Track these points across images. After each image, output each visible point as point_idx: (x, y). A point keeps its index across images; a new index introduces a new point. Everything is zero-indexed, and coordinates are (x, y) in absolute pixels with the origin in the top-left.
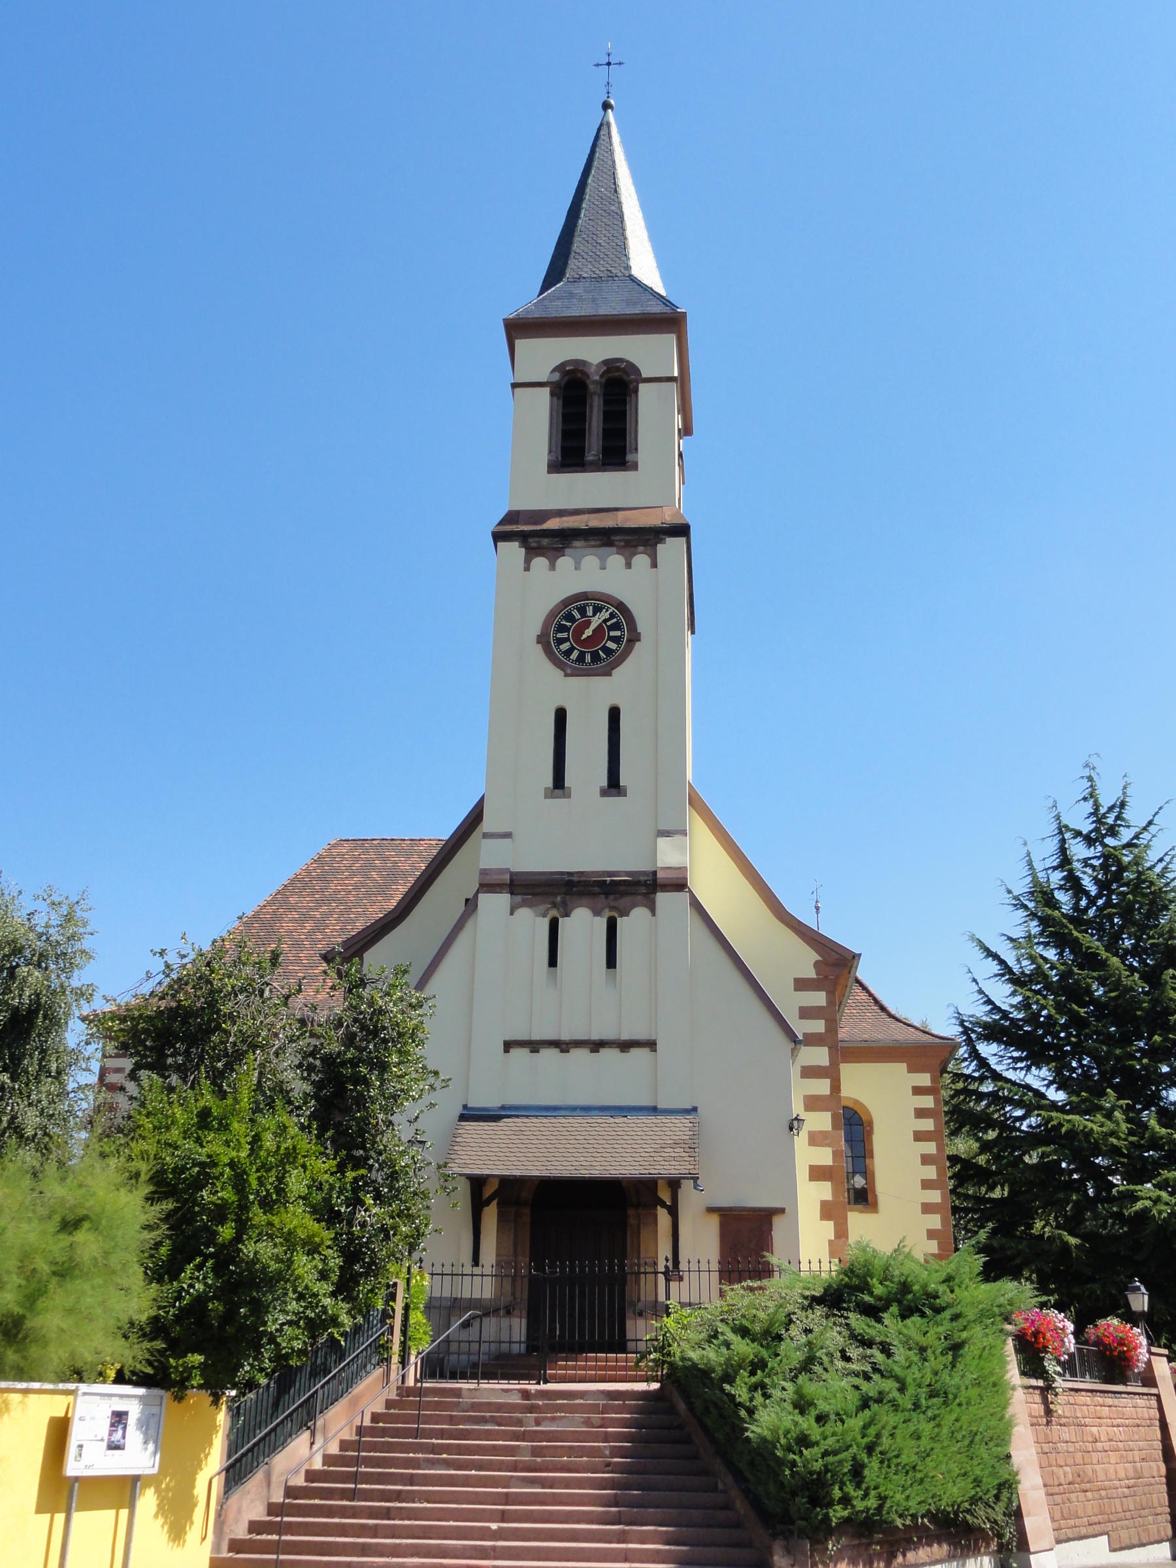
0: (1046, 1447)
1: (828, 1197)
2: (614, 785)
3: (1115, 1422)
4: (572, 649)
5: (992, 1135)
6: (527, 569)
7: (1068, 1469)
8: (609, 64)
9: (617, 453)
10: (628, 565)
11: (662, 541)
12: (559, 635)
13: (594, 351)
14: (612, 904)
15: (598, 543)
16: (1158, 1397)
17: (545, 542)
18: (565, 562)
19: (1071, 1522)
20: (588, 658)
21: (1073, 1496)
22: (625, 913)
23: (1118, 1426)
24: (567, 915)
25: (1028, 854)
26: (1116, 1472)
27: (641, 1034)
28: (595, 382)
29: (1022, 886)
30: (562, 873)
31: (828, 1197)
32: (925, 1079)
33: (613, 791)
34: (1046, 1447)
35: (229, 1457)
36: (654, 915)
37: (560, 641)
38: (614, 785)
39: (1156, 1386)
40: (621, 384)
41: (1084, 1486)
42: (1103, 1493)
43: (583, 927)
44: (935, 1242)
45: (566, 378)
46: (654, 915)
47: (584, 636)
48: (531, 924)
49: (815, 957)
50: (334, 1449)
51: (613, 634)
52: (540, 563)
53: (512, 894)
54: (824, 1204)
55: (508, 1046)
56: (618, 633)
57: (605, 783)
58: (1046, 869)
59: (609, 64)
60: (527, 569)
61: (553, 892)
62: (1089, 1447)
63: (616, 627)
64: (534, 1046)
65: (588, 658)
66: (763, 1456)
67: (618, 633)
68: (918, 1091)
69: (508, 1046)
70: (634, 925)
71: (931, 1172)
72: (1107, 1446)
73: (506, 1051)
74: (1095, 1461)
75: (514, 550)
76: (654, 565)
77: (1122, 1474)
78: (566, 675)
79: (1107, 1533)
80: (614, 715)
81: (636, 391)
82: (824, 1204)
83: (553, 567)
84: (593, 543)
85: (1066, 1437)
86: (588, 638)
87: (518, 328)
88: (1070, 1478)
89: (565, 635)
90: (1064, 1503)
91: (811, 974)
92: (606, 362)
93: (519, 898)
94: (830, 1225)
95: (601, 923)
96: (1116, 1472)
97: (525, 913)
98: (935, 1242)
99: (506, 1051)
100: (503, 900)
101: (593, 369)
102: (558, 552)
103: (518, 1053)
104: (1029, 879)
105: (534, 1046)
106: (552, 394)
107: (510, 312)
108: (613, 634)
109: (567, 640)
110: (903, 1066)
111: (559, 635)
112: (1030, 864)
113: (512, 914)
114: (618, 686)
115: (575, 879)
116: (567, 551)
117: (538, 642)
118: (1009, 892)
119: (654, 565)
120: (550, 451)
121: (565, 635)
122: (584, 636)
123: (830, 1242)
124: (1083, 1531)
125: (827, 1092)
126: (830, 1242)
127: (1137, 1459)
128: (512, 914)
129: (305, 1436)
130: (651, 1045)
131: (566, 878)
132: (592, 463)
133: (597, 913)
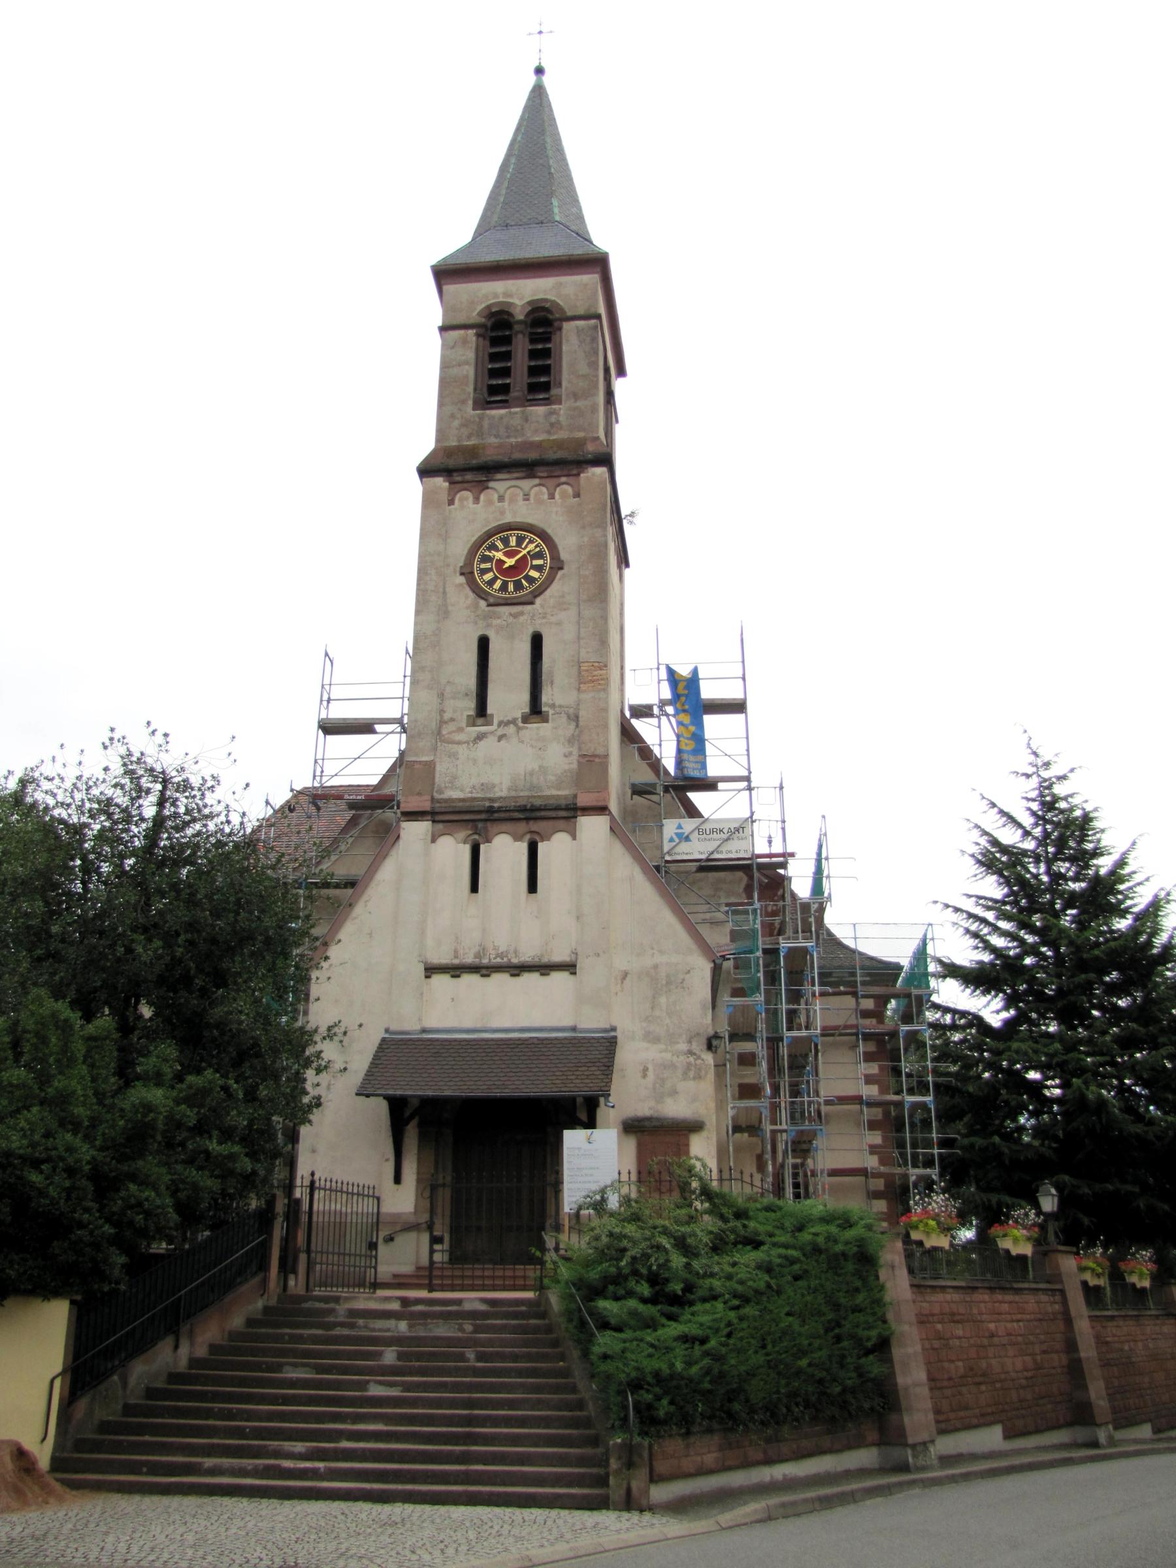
0: (936, 1344)
2: (536, 710)
3: (1014, 1317)
7: (960, 1364)
8: (540, 32)
9: (541, 384)
12: (483, 566)
13: (520, 293)
16: (1062, 1292)
17: (469, 476)
19: (962, 1414)
20: (511, 587)
21: (964, 1389)
22: (546, 837)
23: (1019, 1321)
24: (489, 841)
26: (1013, 1364)
28: (520, 322)
34: (936, 1344)
35: (74, 1360)
37: (484, 572)
38: (536, 710)
39: (1061, 1282)
40: (544, 321)
41: (977, 1380)
42: (998, 1385)
43: (505, 853)
45: (493, 320)
48: (452, 851)
50: (201, 1352)
51: (536, 562)
52: (465, 496)
53: (434, 821)
55: (431, 970)
56: (540, 562)
57: (527, 710)
61: (477, 819)
62: (985, 1342)
63: (539, 555)
65: (511, 587)
66: (689, 1246)
67: (540, 562)
70: (556, 850)
72: (1005, 1340)
74: (991, 1355)
75: (440, 482)
77: (1019, 1366)
79: (1150, 1421)
80: (537, 641)
81: (560, 329)
85: (960, 1333)
87: (445, 274)
88: (962, 1371)
89: (488, 565)
90: (954, 1396)
92: (529, 303)
93: (440, 826)
95: (523, 847)
96: (1013, 1364)
103: (440, 980)
105: (456, 970)
106: (478, 335)
107: (436, 258)
108: (536, 562)
109: (490, 570)
111: (483, 566)
113: (433, 841)
115: (496, 805)
116: (491, 484)
121: (488, 565)
124: (975, 1421)
127: (1038, 1351)
129: (169, 1340)
131: (487, 804)
133: (517, 838)
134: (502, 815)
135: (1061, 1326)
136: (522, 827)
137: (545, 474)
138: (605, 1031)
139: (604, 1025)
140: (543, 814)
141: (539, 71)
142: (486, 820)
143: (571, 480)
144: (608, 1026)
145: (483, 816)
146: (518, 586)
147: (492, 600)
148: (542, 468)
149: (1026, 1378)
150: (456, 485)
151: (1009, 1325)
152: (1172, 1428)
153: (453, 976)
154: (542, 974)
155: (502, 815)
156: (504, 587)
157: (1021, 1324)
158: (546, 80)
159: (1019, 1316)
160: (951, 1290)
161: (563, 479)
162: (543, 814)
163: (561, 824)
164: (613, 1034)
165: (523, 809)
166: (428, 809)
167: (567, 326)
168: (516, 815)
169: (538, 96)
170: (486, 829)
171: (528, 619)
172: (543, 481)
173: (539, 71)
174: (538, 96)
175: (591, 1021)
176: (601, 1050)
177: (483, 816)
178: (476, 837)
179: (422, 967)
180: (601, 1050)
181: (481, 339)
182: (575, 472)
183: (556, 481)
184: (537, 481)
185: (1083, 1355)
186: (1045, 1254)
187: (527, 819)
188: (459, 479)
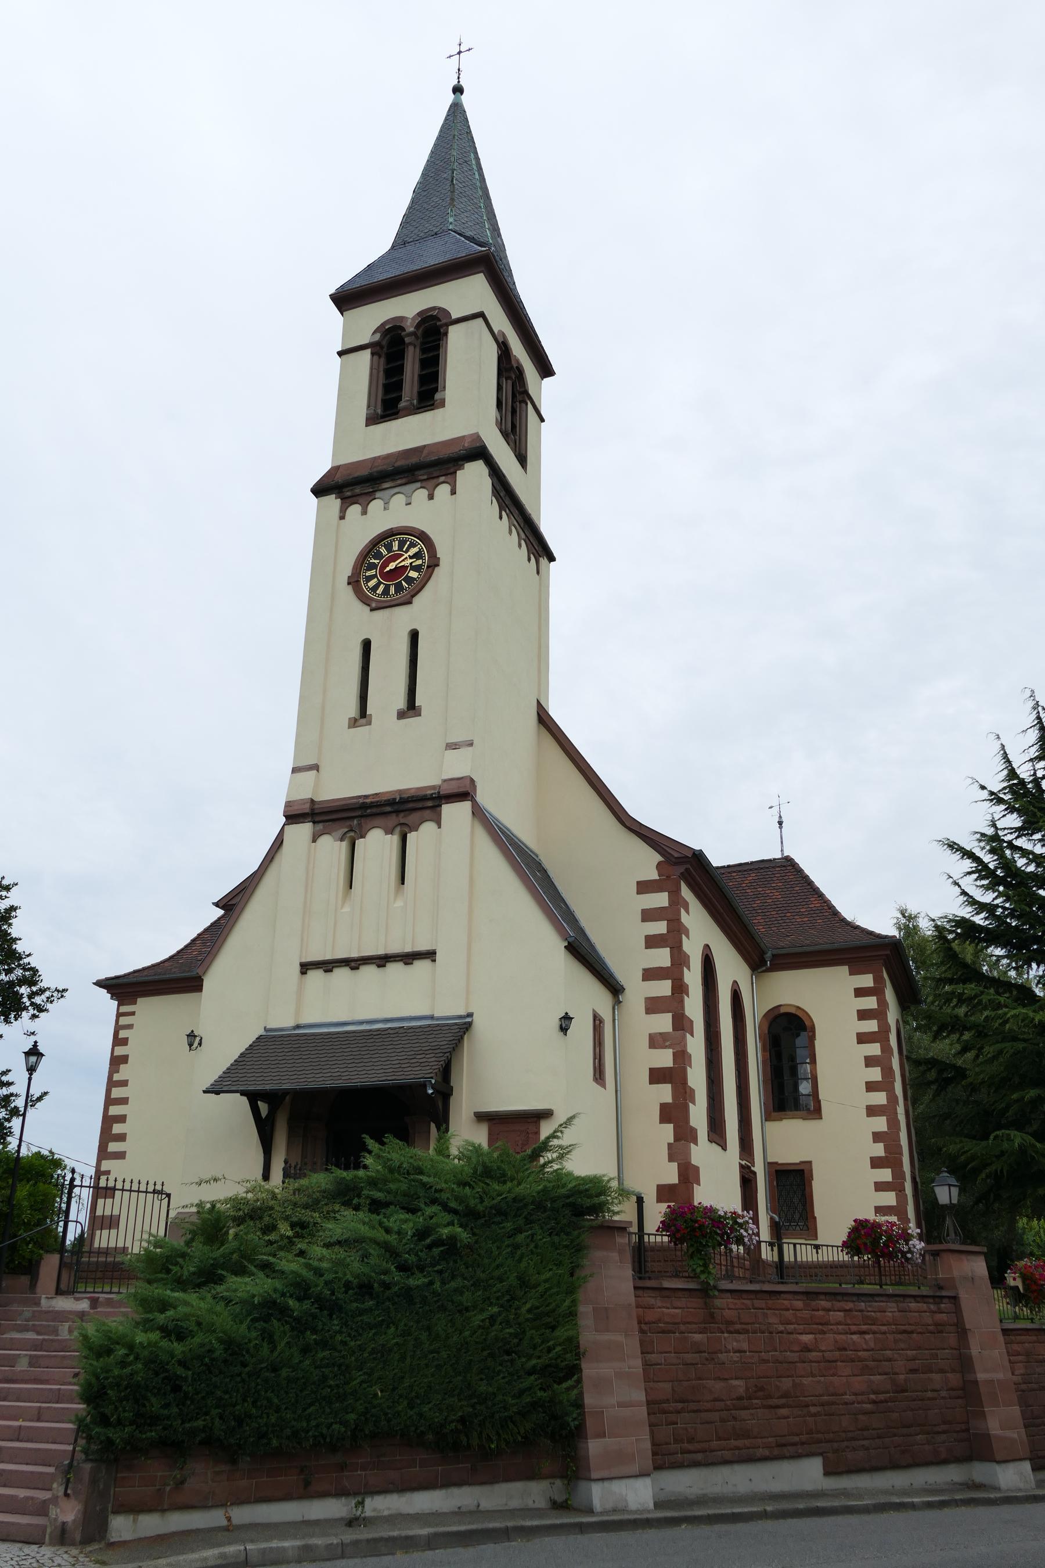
1: (669, 1099)
2: (411, 708)
4: (387, 587)
5: (967, 1036)
6: (342, 518)
10: (431, 497)
11: (461, 467)
13: (408, 307)
14: (402, 821)
15: (403, 481)
18: (376, 506)
20: (392, 590)
24: (363, 836)
25: (1003, 746)
27: (422, 947)
28: (410, 334)
29: (997, 783)
30: (360, 797)
31: (669, 1099)
32: (867, 981)
33: (411, 712)
36: (440, 827)
37: (369, 579)
38: (411, 708)
43: (377, 845)
44: (881, 1145)
46: (440, 827)
47: (388, 569)
48: (331, 848)
49: (659, 858)
52: (355, 510)
53: (314, 822)
54: (663, 1107)
55: (305, 968)
58: (1031, 760)
59: (459, 53)
60: (342, 518)
62: (793, 1356)
64: (328, 966)
65: (392, 590)
68: (860, 992)
69: (305, 968)
70: (423, 838)
71: (875, 1074)
73: (303, 972)
75: (333, 502)
76: (453, 492)
78: (371, 610)
79: (821, 1454)
81: (446, 334)
82: (663, 1107)
83: (364, 512)
84: (399, 482)
86: (389, 573)
91: (654, 875)
92: (419, 314)
93: (320, 826)
94: (670, 1127)
97: (326, 841)
98: (881, 1145)
99: (303, 972)
100: (305, 829)
101: (408, 324)
102: (370, 496)
103: (316, 976)
104: (1005, 772)
105: (328, 966)
109: (375, 576)
110: (845, 969)
112: (1005, 756)
113: (314, 841)
114: (415, 614)
115: (368, 801)
116: (378, 494)
117: (349, 584)
118: (983, 788)
119: (453, 492)
120: (369, 406)
121: (373, 572)
122: (388, 569)
123: (669, 1144)
125: (668, 992)
126: (669, 1144)
128: (314, 841)
130: (430, 955)
131: (361, 801)
132: (405, 408)
133: (389, 831)
134: (374, 810)
135: (952, 1339)
136: (393, 820)
137: (425, 477)
138: (460, 1017)
139: (462, 1012)
140: (411, 805)
141: (458, 90)
142: (361, 816)
143: (449, 478)
144: (463, 1013)
145: (359, 813)
146: (399, 588)
147: (374, 605)
148: (422, 472)
149: (874, 1402)
150: (347, 501)
151: (838, 1337)
152: (2, 1522)
153: (326, 971)
154: (406, 964)
155: (374, 810)
156: (386, 592)
157: (867, 1337)
158: (467, 100)
159: (864, 1327)
160: (728, 1295)
161: (442, 479)
162: (411, 805)
163: (427, 813)
164: (469, 1020)
165: (391, 802)
166: (307, 811)
167: (452, 329)
168: (388, 809)
169: (456, 116)
170: (360, 825)
171: (403, 619)
172: (424, 484)
173: (458, 90)
174: (456, 116)
175: (448, 1008)
176: (448, 1040)
177: (359, 813)
178: (352, 834)
179: (438, 957)
180: (448, 1040)
181: (376, 357)
182: (452, 470)
183: (435, 481)
184: (418, 485)
185: (981, 1376)
186: (936, 1254)
187: (397, 812)
188: (349, 494)
